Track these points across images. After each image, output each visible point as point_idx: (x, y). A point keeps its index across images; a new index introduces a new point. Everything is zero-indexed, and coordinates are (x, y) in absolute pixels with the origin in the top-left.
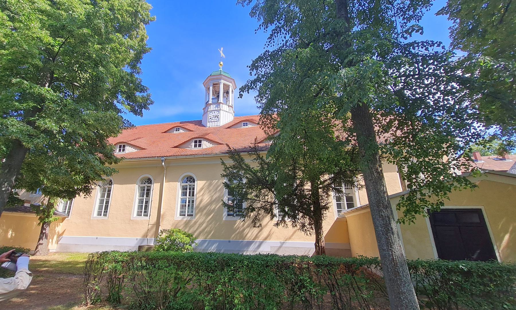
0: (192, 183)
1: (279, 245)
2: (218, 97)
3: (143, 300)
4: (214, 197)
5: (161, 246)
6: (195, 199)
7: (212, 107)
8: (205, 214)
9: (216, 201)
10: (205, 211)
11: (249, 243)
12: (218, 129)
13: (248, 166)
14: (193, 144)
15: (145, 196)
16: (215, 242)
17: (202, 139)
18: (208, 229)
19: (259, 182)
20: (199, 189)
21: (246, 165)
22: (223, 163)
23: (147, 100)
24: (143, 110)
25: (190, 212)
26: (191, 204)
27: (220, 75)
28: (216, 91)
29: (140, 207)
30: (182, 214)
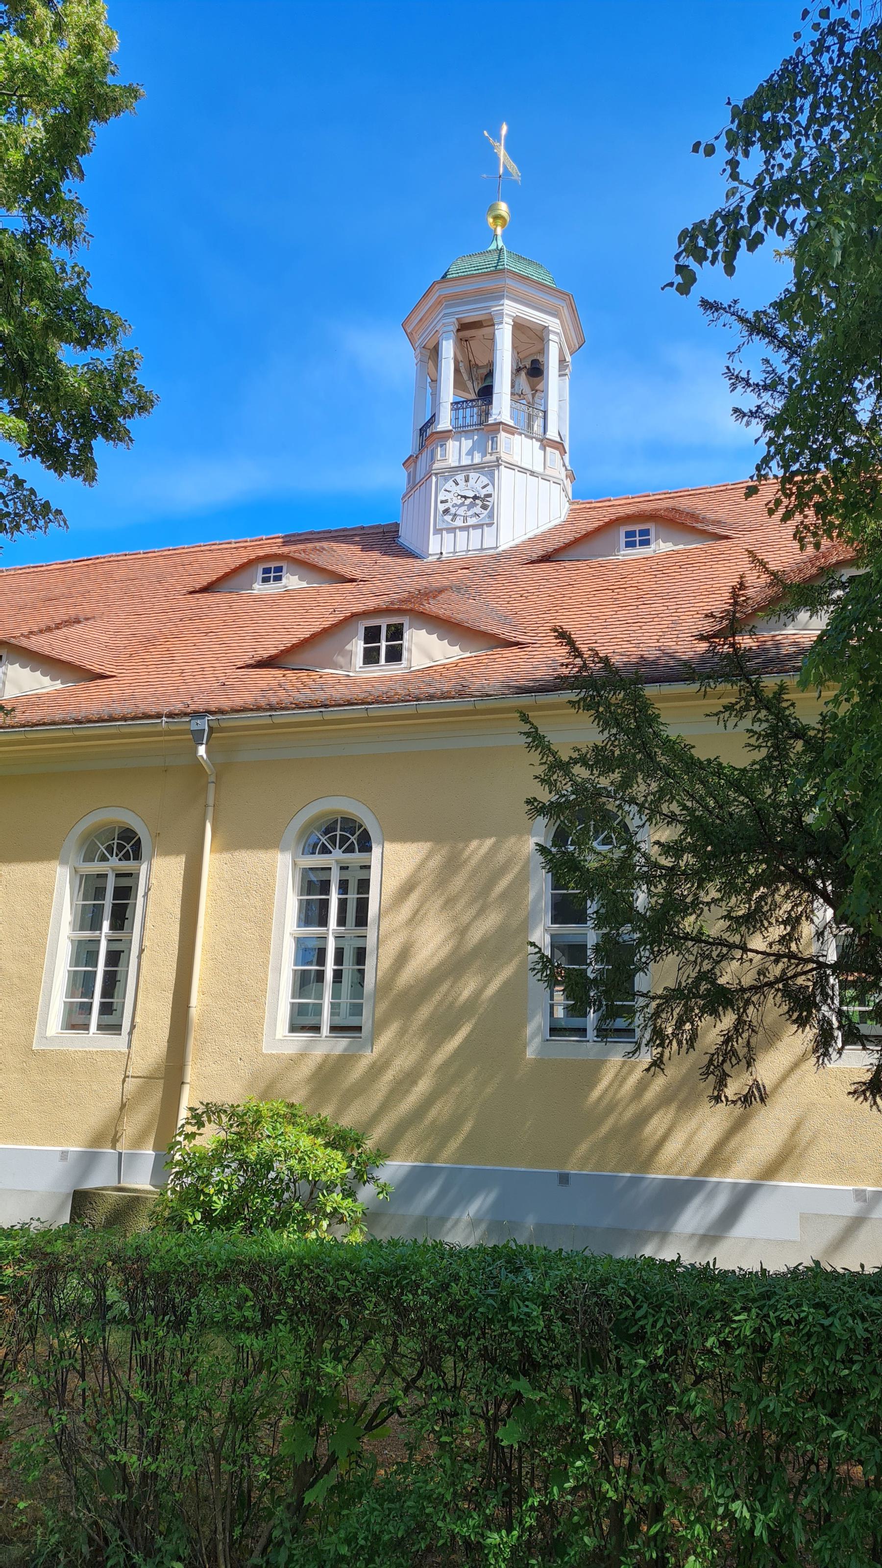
0: (357, 857)
1: (852, 1208)
2: (486, 393)
3: (117, 1524)
4: (476, 935)
5: (193, 1197)
6: (371, 943)
7: (455, 452)
8: (427, 1024)
9: (490, 952)
10: (425, 1012)
11: (677, 1195)
12: (493, 565)
13: (681, 754)
14: (358, 646)
15: (106, 925)
16: (475, 1183)
17: (405, 621)
18: (439, 1111)
19: (748, 843)
20: (392, 884)
21: (669, 746)
22: (537, 740)
23: (116, 388)
24: (99, 444)
25: (344, 1009)
26: (348, 967)
27: (498, 271)
28: (472, 367)
29: (82, 983)
30: (303, 1021)
